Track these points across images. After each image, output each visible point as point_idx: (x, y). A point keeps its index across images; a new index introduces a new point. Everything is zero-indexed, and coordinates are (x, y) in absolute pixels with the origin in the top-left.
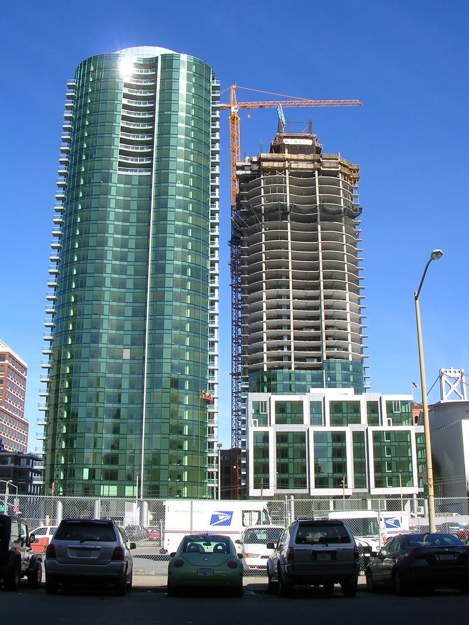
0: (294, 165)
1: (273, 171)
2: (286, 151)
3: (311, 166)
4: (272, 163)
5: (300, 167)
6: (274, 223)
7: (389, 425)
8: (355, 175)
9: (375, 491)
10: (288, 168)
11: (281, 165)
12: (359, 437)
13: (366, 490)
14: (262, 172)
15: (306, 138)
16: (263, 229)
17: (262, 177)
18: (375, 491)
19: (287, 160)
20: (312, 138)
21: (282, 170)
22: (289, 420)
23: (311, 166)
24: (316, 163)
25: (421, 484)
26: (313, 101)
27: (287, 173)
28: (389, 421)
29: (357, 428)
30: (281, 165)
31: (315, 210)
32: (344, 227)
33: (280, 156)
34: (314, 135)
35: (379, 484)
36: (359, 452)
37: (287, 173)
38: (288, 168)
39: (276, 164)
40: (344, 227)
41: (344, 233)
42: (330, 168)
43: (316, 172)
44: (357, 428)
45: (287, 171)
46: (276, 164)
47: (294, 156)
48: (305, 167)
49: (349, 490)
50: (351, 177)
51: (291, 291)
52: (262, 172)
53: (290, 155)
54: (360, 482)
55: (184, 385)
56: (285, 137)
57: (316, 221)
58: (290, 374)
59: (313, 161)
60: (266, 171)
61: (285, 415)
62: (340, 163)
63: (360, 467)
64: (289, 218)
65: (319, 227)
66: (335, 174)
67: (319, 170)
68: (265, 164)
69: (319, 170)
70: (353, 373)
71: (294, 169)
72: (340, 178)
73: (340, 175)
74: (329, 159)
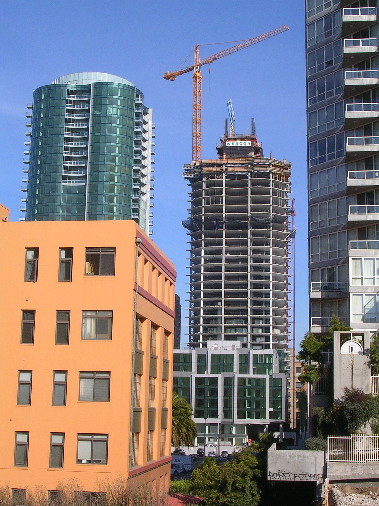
0: (229, 169)
1: (213, 175)
3: (243, 169)
4: (211, 168)
7: (254, 373)
9: (237, 421)
11: (218, 169)
12: (228, 382)
13: (231, 420)
14: (204, 175)
17: (204, 179)
18: (237, 421)
21: (220, 174)
22: (181, 368)
23: (243, 169)
25: (317, 440)
27: (224, 177)
28: (254, 369)
29: (228, 375)
30: (218, 169)
35: (241, 415)
36: (228, 392)
37: (224, 177)
39: (215, 169)
44: (228, 375)
46: (215, 169)
47: (230, 161)
49: (219, 420)
52: (204, 175)
54: (227, 414)
55: (206, 393)
60: (207, 175)
61: (179, 364)
63: (228, 403)
66: (267, 175)
67: (251, 172)
68: (205, 170)
69: (252, 173)
71: (230, 172)
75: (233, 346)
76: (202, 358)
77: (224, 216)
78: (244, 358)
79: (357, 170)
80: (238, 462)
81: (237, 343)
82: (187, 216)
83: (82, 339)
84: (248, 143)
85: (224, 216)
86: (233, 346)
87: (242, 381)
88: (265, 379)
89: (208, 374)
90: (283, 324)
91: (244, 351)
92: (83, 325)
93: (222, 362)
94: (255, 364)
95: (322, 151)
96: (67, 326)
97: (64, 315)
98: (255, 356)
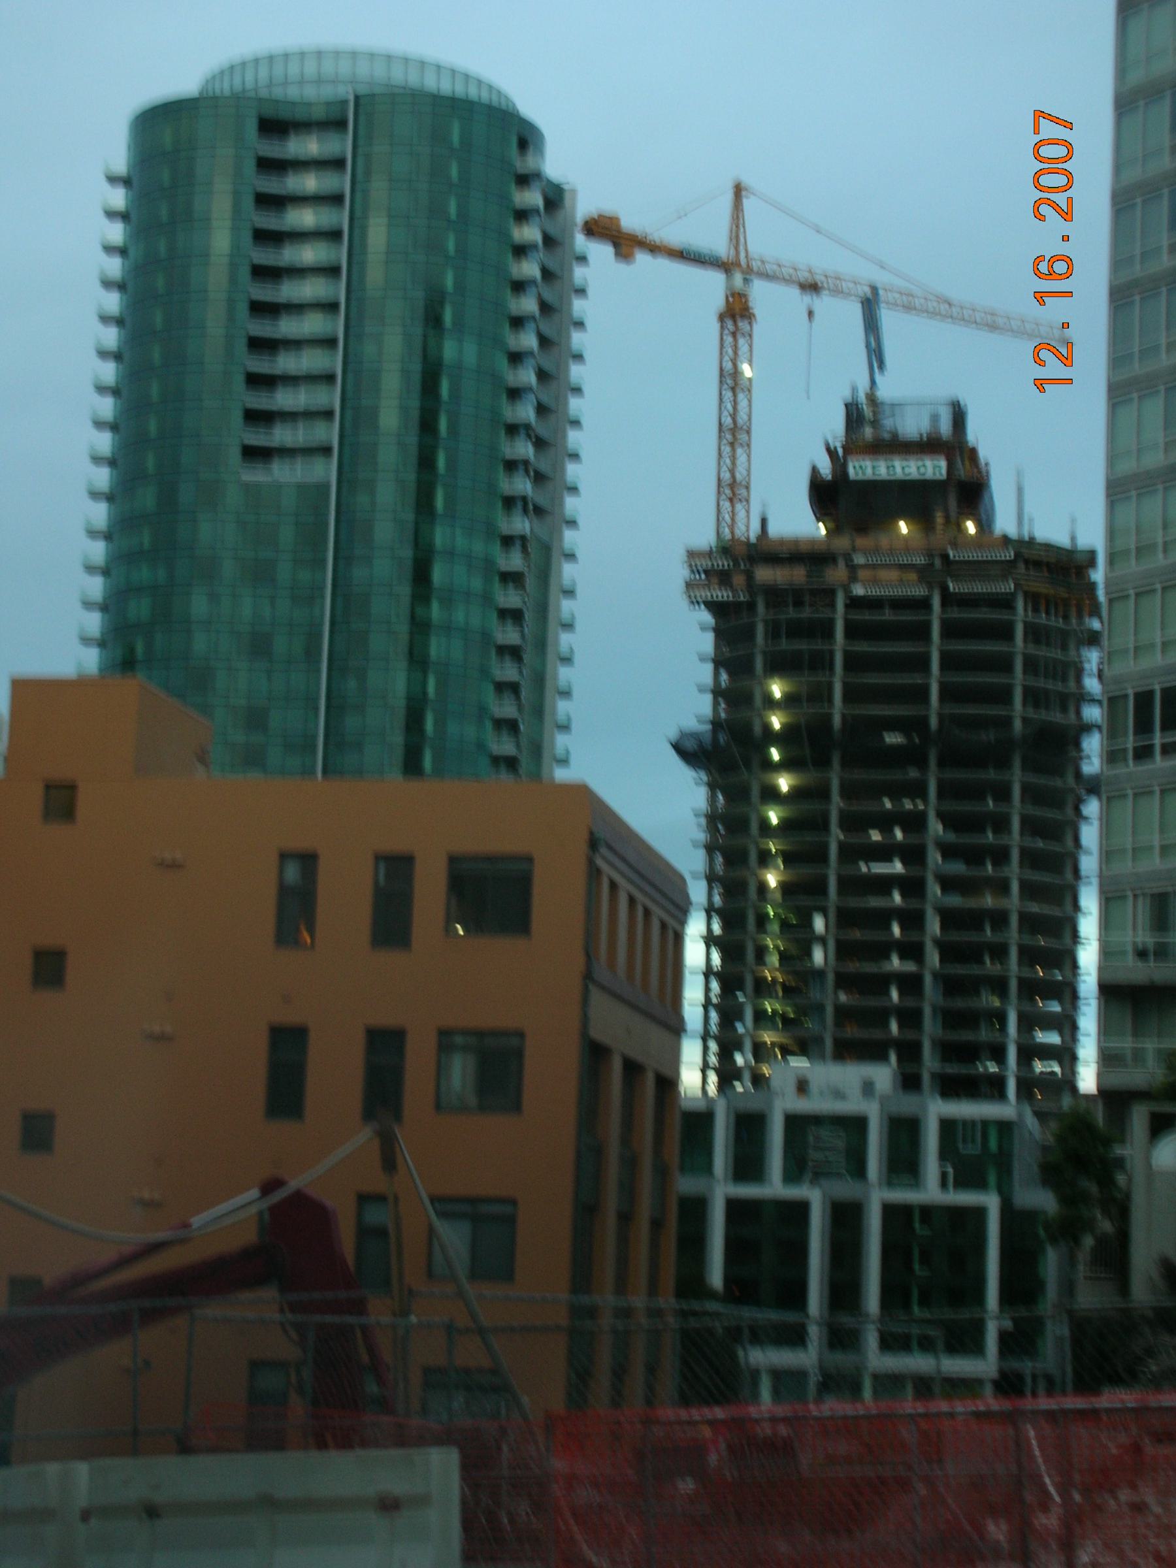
7: (944, 1184)
12: (846, 1216)
29: (845, 1189)
36: (844, 1293)
54: (842, 1338)
63: (844, 1293)
75: (868, 1088)
76: (750, 1126)
77: (837, 720)
78: (904, 1131)
79: (1109, 991)
80: (255, 719)
81: (883, 1075)
82: (695, 709)
83: (438, 1107)
84: (933, 468)
85: (837, 720)
86: (868, 1088)
87: (894, 1214)
88: (980, 1213)
89: (774, 1186)
90: (922, 1263)
91: (907, 1105)
92: (441, 1070)
93: (821, 1141)
94: (947, 1152)
95: (1143, 726)
96: (397, 1073)
97: (384, 1044)
98: (948, 1126)
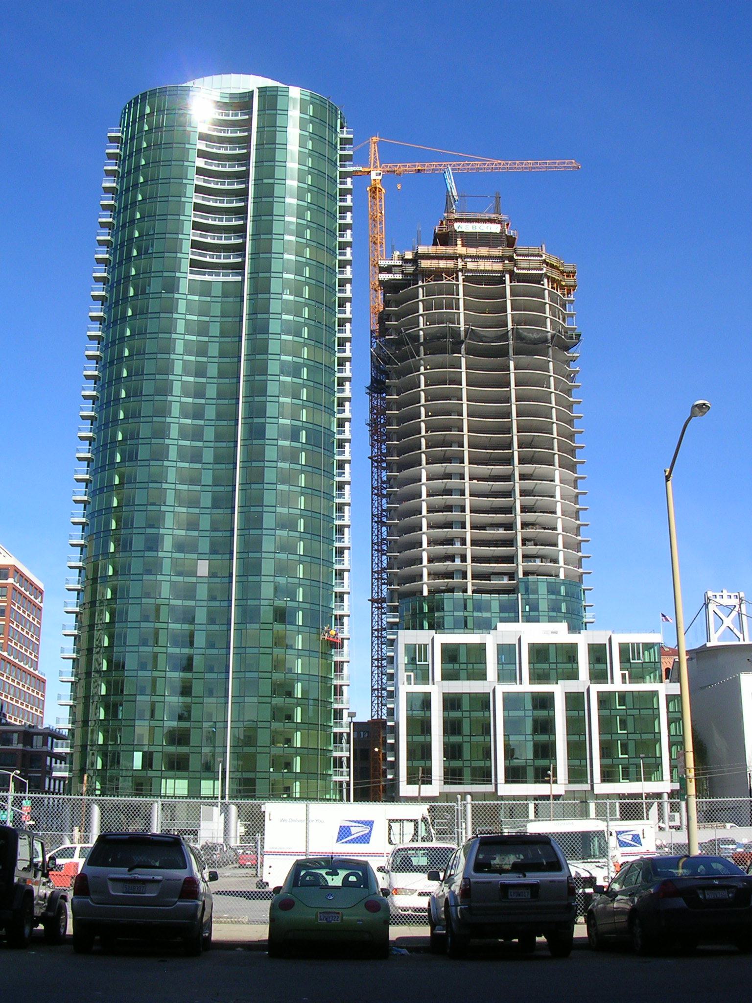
0: (471, 265)
1: (437, 274)
2: (459, 242)
3: (498, 266)
4: (436, 261)
5: (482, 268)
6: (439, 358)
7: (624, 682)
8: (570, 281)
9: (602, 788)
10: (461, 270)
11: (450, 264)
12: (575, 701)
13: (586, 787)
14: (420, 276)
15: (490, 221)
16: (422, 368)
17: (420, 283)
18: (602, 788)
19: (461, 256)
20: (500, 222)
21: (452, 273)
22: (463, 674)
23: (498, 266)
24: (506, 262)
25: (675, 777)
26: (502, 162)
27: (461, 278)
28: (624, 676)
29: (572, 686)
30: (450, 264)
31: (504, 337)
32: (551, 364)
33: (450, 250)
34: (504, 217)
35: (608, 776)
36: (576, 725)
37: (461, 278)
38: (461, 270)
39: (443, 264)
40: (551, 364)
41: (552, 374)
42: (529, 269)
43: (507, 276)
44: (572, 686)
45: (460, 274)
46: (443, 264)
47: (472, 251)
48: (489, 268)
49: (560, 787)
50: (564, 283)
51: (467, 467)
52: (420, 276)
53: (464, 249)
54: (577, 774)
55: (295, 617)
56: (457, 220)
57: (506, 354)
58: (465, 600)
59: (501, 259)
60: (427, 274)
61: (457, 666)
62: (544, 261)
63: (577, 749)
64: (463, 350)
65: (512, 364)
66: (538, 279)
67: (511, 273)
68: (425, 264)
69: (511, 273)
70: (567, 598)
71: (471, 271)
72: (546, 286)
73: (546, 280)
74: (527, 255)
